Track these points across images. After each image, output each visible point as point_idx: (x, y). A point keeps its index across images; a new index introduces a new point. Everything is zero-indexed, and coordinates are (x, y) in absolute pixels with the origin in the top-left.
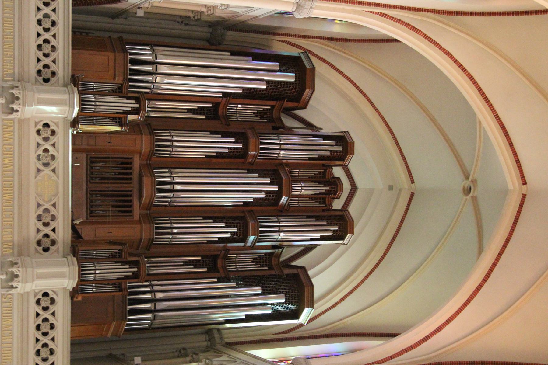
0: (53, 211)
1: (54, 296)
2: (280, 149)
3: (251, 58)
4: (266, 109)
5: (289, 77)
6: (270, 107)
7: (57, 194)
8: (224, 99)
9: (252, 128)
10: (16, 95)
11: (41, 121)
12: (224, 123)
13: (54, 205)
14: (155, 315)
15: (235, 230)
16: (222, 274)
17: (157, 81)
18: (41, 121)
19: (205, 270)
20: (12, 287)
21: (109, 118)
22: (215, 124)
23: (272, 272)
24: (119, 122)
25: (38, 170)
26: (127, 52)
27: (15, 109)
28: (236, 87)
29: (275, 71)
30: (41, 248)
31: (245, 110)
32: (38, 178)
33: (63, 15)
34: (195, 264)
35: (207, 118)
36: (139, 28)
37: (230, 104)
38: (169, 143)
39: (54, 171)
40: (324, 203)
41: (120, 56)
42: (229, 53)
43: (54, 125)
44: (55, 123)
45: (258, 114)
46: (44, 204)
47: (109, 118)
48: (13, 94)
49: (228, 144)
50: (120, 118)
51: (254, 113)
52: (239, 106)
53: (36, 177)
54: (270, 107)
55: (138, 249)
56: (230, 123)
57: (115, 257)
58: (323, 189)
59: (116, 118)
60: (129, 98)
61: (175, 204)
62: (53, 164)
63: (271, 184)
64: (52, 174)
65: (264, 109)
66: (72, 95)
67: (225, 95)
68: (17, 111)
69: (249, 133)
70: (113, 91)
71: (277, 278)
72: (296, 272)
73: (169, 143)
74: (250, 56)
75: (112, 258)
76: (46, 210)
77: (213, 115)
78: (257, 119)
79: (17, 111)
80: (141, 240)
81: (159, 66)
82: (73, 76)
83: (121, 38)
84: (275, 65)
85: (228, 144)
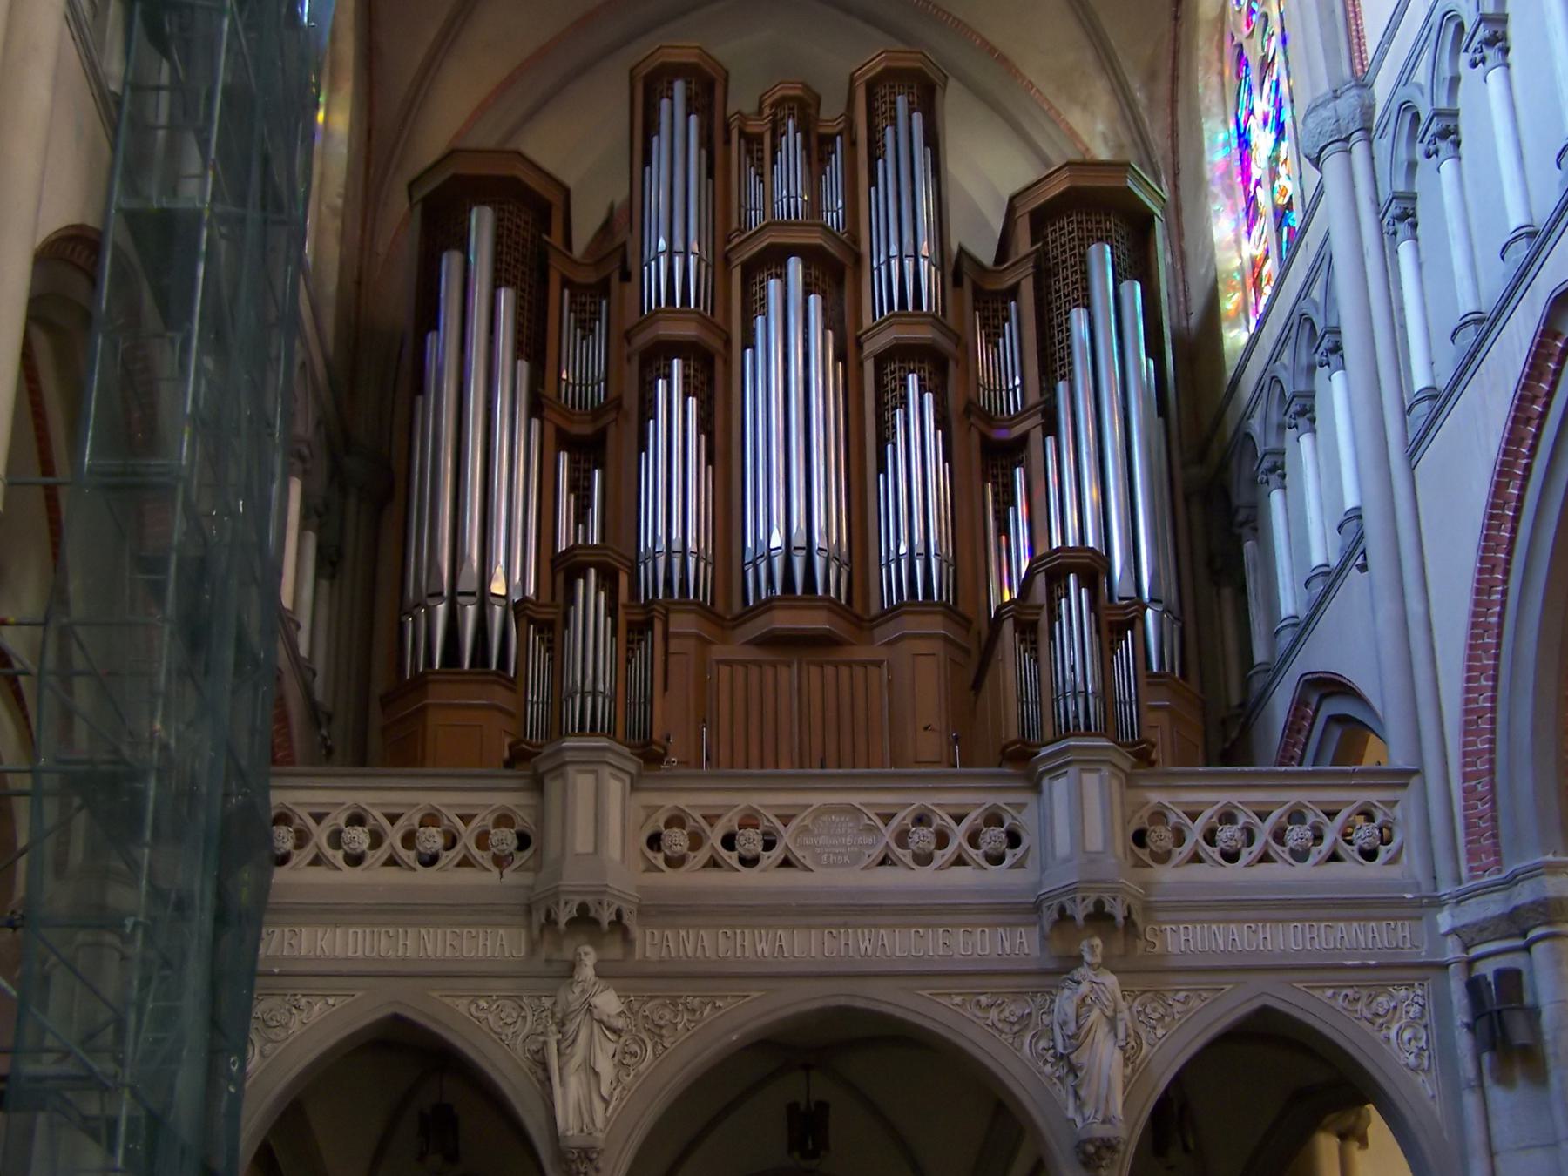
0: (903, 818)
1: (1145, 813)
2: (595, 693)
3: (431, 337)
4: (571, 303)
5: (481, 223)
6: (566, 292)
7: (853, 811)
8: (547, 413)
9: (628, 336)
10: (574, 913)
11: (643, 854)
12: (613, 415)
13: (887, 818)
14: (1152, 600)
15: (913, 380)
16: (1033, 424)
17: (502, 592)
18: (643, 854)
19: (1019, 472)
20: (1128, 918)
21: (629, 661)
22: (619, 440)
23: (1027, 289)
24: (641, 632)
25: (786, 863)
26: (424, 674)
27: (613, 917)
28: (512, 374)
29: (466, 262)
30: (1009, 853)
31: (582, 362)
32: (808, 862)
33: (319, 793)
34: (1006, 498)
35: (601, 465)
36: (328, 58)
37: (559, 396)
38: (677, 561)
39: (786, 820)
40: (831, 139)
41: (437, 694)
42: (420, 399)
43: (654, 818)
44: (648, 817)
45: (585, 327)
46: (882, 846)
47: (629, 661)
48: (571, 922)
49: (675, 411)
50: (631, 626)
51: (583, 338)
52: (564, 376)
53: (808, 869)
54: (566, 292)
55: (967, 652)
56: (613, 394)
57: (1035, 642)
58: (792, 140)
59: (629, 642)
60: (571, 599)
61: (844, 549)
62: (771, 820)
63: (783, 277)
64: (794, 824)
65: (570, 311)
66: (568, 756)
67: (536, 407)
68: (619, 913)
69: (641, 340)
70: (548, 650)
71: (1044, 274)
72: (1027, 218)
73: (677, 561)
74: (424, 342)
75: (1036, 650)
76: (902, 838)
77: (590, 442)
78: (600, 327)
79: (619, 913)
80: (945, 638)
81: (461, 588)
82: (508, 764)
83: (387, 701)
84: (450, 263)
85: (675, 411)
